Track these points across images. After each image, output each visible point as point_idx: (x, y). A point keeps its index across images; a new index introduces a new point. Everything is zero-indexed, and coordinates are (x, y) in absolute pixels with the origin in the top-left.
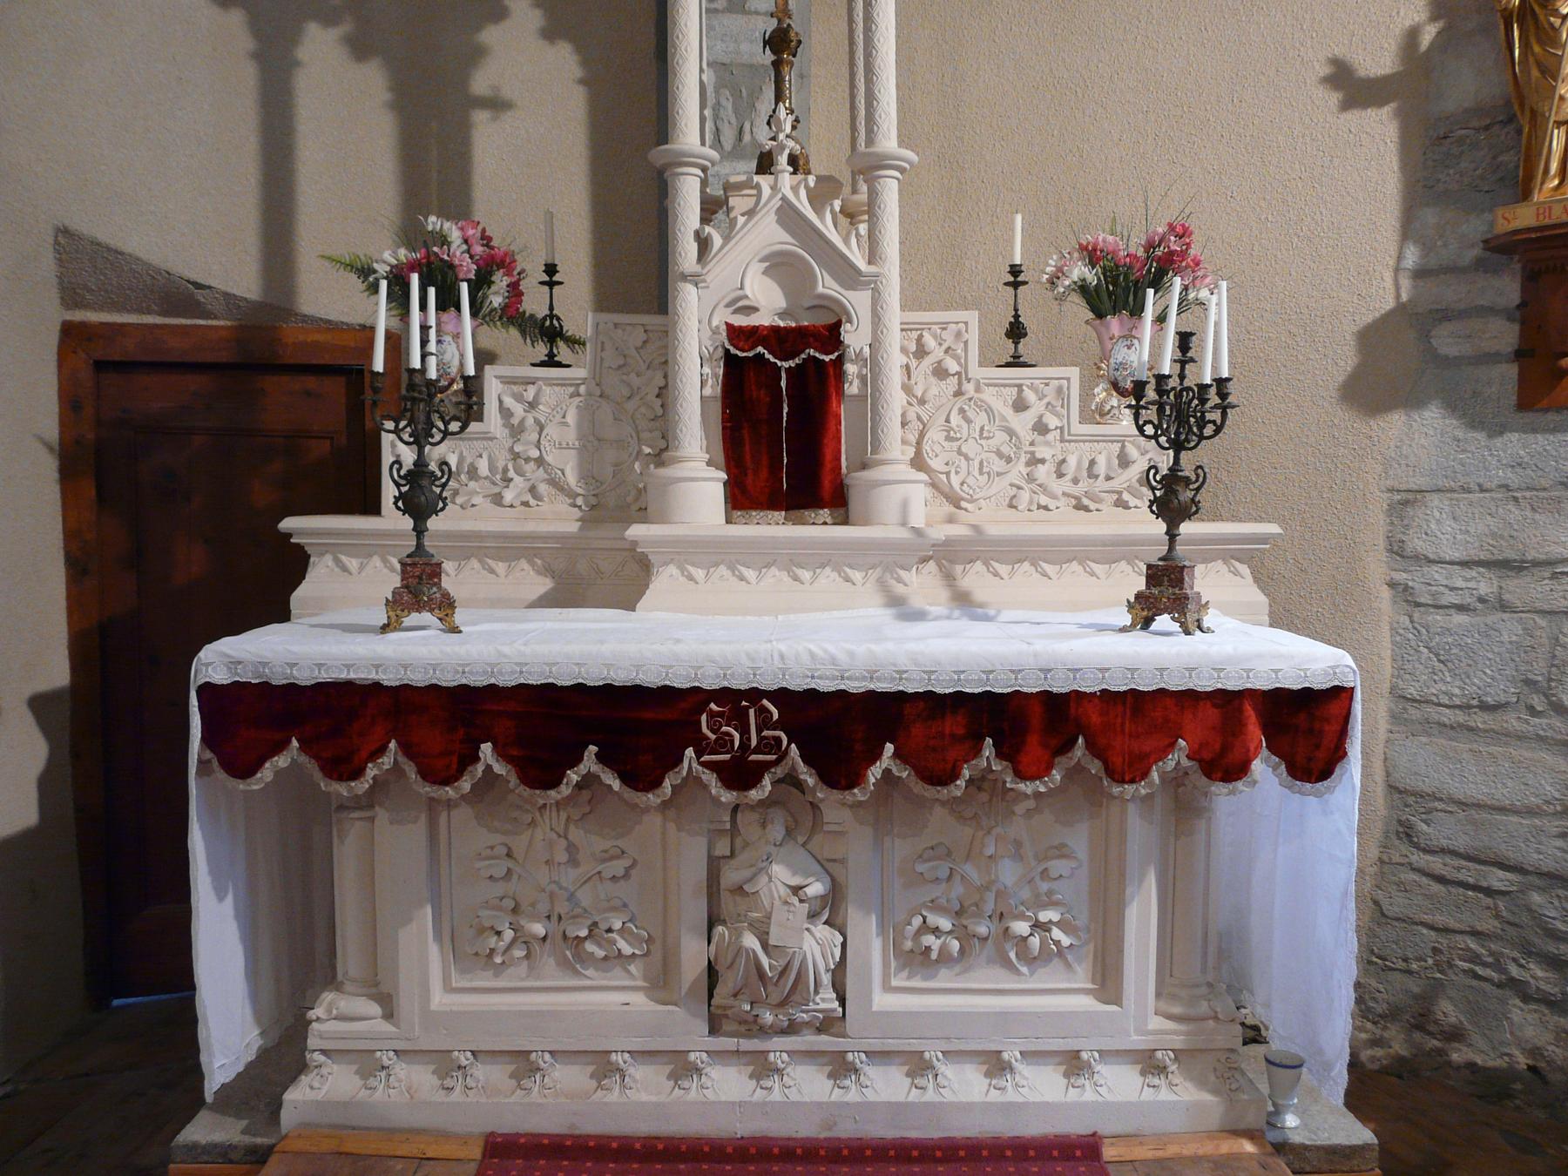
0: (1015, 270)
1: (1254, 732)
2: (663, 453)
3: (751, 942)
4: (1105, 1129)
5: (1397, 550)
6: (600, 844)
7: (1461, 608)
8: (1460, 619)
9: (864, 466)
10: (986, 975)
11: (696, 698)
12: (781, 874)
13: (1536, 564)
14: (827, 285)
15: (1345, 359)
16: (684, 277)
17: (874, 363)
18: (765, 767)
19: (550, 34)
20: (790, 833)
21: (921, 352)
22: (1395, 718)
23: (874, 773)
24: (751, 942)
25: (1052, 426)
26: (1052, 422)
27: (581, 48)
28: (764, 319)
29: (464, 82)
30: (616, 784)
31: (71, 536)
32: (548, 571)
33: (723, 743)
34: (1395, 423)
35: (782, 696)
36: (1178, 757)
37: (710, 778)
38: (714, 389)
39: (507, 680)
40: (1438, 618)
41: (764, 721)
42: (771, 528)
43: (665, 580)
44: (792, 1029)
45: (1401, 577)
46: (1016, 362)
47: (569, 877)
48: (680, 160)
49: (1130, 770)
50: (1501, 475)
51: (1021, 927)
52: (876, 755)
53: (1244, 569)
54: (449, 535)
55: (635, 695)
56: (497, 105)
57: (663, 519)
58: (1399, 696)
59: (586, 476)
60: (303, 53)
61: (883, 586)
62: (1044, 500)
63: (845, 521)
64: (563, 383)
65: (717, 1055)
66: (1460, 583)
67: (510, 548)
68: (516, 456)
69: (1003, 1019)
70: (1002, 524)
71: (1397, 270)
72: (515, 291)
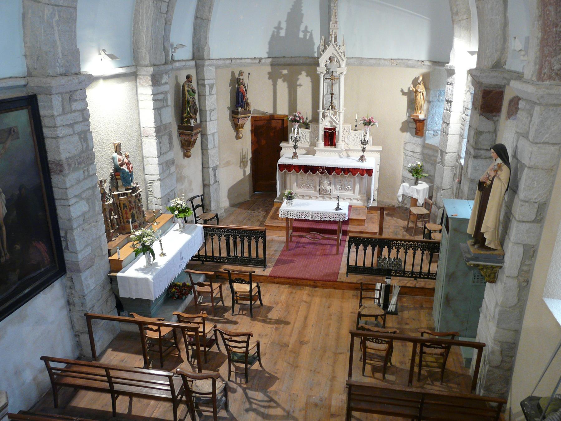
2: (318, 140)
3: (323, 187)
5: (404, 149)
8: (410, 157)
10: (343, 191)
11: (319, 167)
12: (326, 181)
14: (334, 124)
15: (401, 126)
19: (307, 76)
22: (403, 168)
24: (323, 187)
26: (358, 137)
27: (311, 77)
28: (328, 127)
29: (296, 83)
31: (252, 140)
32: (306, 150)
35: (325, 167)
38: (323, 134)
39: (303, 165)
40: (407, 157)
42: (329, 148)
43: (317, 153)
44: (326, 195)
46: (356, 130)
47: (308, 181)
49: (354, 174)
50: (414, 142)
51: (346, 187)
52: (333, 172)
55: (313, 166)
56: (300, 85)
57: (317, 147)
58: (404, 166)
59: (310, 141)
65: (320, 197)
67: (302, 148)
69: (344, 195)
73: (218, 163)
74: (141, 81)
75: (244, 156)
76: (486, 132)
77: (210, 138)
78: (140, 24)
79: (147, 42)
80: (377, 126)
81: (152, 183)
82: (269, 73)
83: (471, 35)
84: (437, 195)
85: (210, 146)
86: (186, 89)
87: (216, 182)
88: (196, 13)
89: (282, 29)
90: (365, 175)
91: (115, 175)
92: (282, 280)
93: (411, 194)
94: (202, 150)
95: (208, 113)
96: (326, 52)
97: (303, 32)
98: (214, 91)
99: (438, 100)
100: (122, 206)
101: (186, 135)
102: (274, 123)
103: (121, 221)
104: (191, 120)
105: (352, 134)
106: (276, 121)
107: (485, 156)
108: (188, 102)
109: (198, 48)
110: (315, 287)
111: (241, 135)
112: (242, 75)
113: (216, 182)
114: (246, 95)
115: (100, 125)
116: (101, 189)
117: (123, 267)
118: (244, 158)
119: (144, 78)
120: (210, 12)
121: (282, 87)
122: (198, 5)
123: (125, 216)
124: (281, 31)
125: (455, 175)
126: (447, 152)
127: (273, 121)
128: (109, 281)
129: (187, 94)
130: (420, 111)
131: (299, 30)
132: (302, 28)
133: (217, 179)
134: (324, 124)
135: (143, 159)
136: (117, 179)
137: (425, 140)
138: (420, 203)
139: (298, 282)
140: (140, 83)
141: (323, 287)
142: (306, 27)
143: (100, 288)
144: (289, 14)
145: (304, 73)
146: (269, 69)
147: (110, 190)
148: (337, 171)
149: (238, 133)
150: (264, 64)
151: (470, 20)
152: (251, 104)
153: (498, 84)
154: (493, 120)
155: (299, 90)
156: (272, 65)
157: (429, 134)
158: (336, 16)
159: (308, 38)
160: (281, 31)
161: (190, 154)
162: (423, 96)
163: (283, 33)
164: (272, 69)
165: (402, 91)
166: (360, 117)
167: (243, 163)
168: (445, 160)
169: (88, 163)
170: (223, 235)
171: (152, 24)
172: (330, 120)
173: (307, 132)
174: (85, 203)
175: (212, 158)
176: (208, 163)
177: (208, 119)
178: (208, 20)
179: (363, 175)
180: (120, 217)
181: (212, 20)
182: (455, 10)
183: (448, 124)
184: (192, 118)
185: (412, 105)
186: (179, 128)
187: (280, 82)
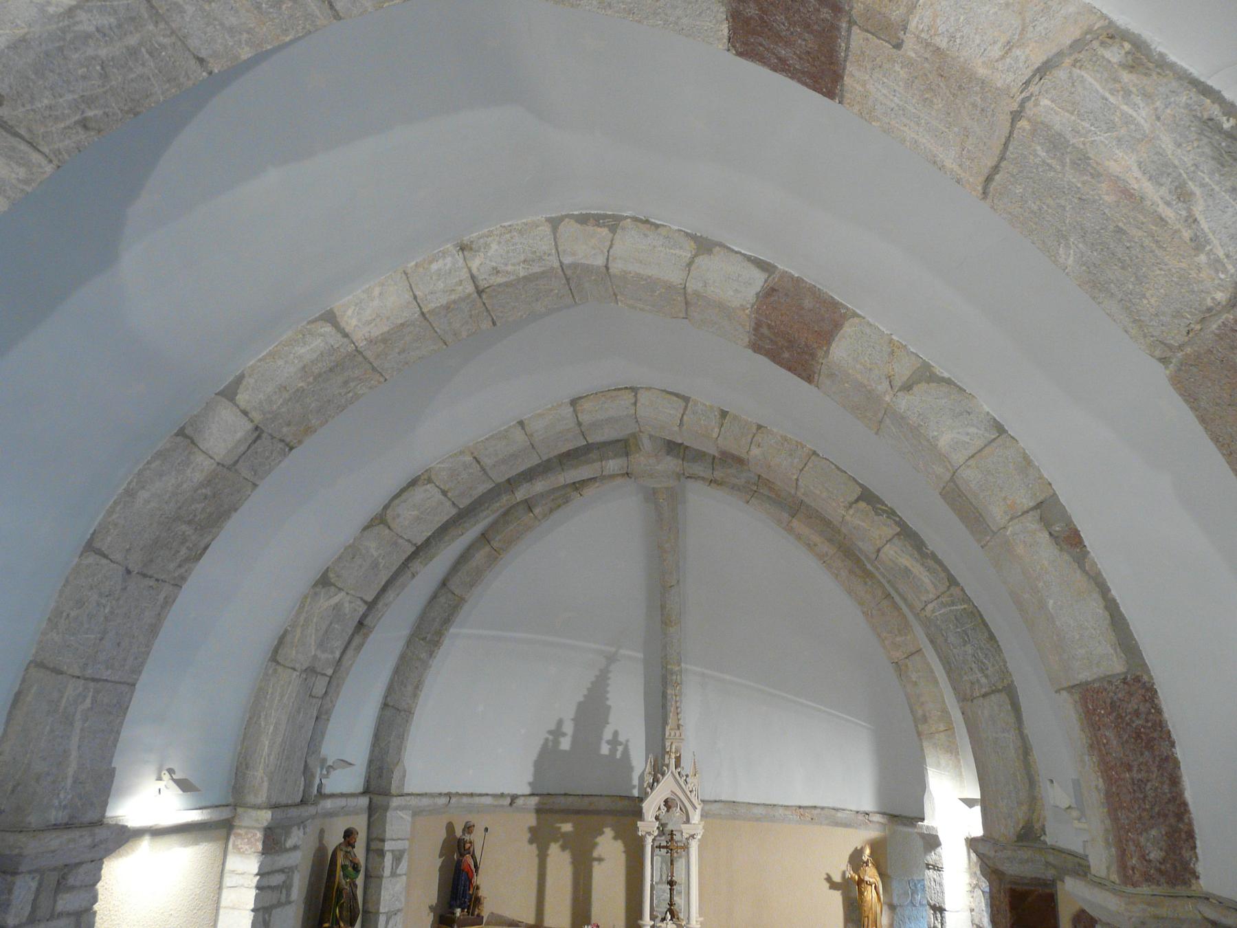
19: (615, 838)
25: (1136, 707)
29: (591, 853)
56: (600, 860)
60: (549, 852)
74: (239, 842)
79: (269, 755)
82: (531, 830)
88: (386, 697)
89: (564, 735)
96: (659, 788)
97: (608, 742)
98: (403, 867)
108: (340, 891)
109: (381, 768)
112: (470, 833)
114: (474, 880)
120: (415, 696)
121: (560, 863)
124: (562, 739)
129: (339, 873)
132: (607, 734)
142: (616, 734)
145: (609, 832)
146: (532, 820)
155: (598, 871)
159: (618, 755)
163: (565, 744)
165: (829, 879)
182: (920, 713)
187: (554, 849)
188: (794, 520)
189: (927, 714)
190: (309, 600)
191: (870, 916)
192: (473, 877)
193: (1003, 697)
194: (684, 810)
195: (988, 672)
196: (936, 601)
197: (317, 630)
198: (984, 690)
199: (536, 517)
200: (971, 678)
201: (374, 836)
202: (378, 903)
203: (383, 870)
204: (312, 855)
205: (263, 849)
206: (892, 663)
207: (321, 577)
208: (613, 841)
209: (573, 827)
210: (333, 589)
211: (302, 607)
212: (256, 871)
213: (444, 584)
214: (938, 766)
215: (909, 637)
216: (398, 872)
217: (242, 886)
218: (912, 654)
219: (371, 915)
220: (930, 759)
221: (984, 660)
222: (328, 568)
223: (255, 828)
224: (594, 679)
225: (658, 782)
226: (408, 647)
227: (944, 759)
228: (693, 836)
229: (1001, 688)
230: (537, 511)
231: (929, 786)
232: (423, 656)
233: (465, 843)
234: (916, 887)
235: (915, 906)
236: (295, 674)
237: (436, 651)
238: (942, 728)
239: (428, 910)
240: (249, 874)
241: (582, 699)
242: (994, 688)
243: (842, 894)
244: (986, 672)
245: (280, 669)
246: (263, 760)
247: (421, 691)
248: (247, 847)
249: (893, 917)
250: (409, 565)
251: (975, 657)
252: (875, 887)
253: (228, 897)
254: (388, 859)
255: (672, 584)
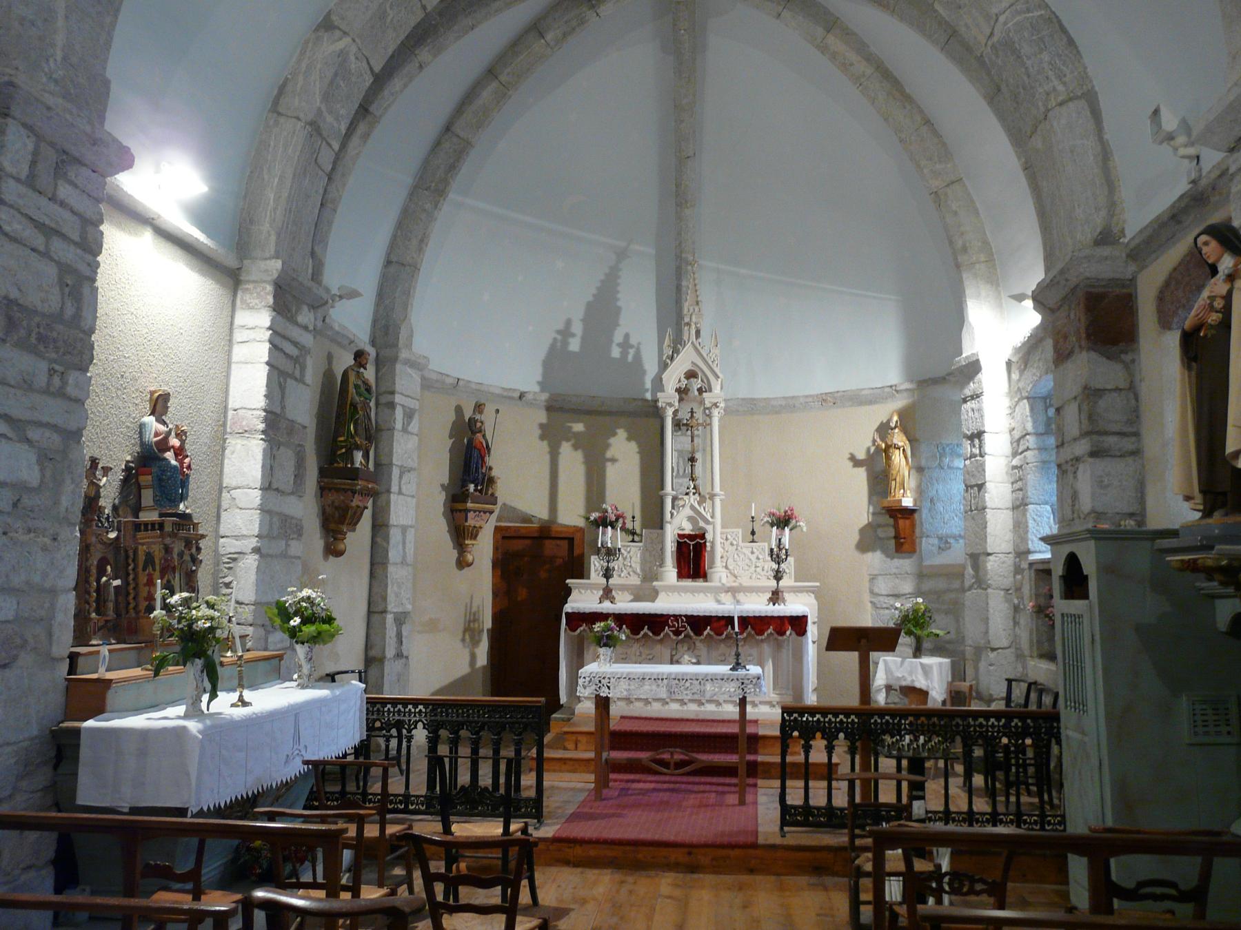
0: (753, 518)
1: (786, 622)
2: (662, 564)
4: (760, 718)
5: (872, 592)
6: (647, 652)
7: (887, 608)
8: (887, 611)
9: (711, 568)
11: (668, 616)
13: (903, 595)
14: (702, 524)
15: (856, 537)
16: (667, 522)
17: (713, 543)
18: (682, 631)
19: (629, 439)
20: (689, 649)
21: (727, 539)
23: (705, 633)
26: (761, 557)
27: (636, 441)
28: (687, 532)
30: (651, 634)
31: (493, 585)
32: (631, 594)
33: (674, 626)
34: (870, 555)
35: (686, 616)
36: (770, 630)
37: (671, 634)
38: (674, 549)
40: (882, 612)
41: (682, 621)
42: (688, 583)
43: (662, 596)
45: (873, 600)
46: (753, 541)
48: (666, 495)
50: (894, 570)
52: (706, 629)
53: (813, 595)
54: (614, 585)
56: (613, 460)
57: (662, 580)
59: (642, 570)
61: (715, 596)
62: (759, 577)
63: (707, 581)
64: (637, 547)
66: (886, 601)
68: (625, 565)
70: (745, 582)
71: (868, 512)
72: (624, 523)
73: (409, 607)
74: (247, 297)
75: (474, 614)
76: (1110, 390)
77: (395, 535)
78: (265, 171)
79: (275, 209)
80: (805, 529)
81: (234, 560)
82: (542, 426)
83: (1001, 299)
84: (977, 669)
85: (393, 555)
86: (352, 378)
87: (399, 655)
88: (388, 254)
89: (573, 335)
90: (788, 633)
91: (137, 474)
92: (593, 852)
93: (909, 679)
94: (372, 564)
95: (395, 472)
96: (679, 359)
97: (619, 345)
98: (414, 426)
99: (939, 464)
100: (142, 557)
101: (338, 490)
102: (549, 547)
103: (129, 603)
104: (355, 452)
105: (744, 550)
106: (554, 542)
107: (1120, 450)
108: (354, 406)
109: (387, 327)
110: (693, 868)
111: (470, 558)
112: (481, 412)
113: (399, 655)
114: (487, 458)
115: (122, 326)
116: (92, 483)
117: (108, 708)
118: (474, 621)
119: (255, 288)
120: (420, 250)
121: (572, 462)
122: (394, 237)
123: (144, 592)
124: (571, 340)
125: (1016, 609)
126: (989, 551)
127: (547, 542)
128: (53, 753)
129: (352, 390)
130: (902, 491)
131: (610, 341)
132: (618, 337)
133: (404, 647)
134: (678, 524)
135: (220, 492)
136: (139, 488)
137: (921, 559)
138: (935, 700)
139: (640, 856)
140: (243, 301)
141: (717, 868)
142: (627, 336)
143: (13, 761)
144: (589, 305)
145: (622, 434)
146: (542, 417)
147: (115, 508)
148: (715, 625)
149: (461, 547)
150: (531, 404)
151: (995, 265)
152: (498, 481)
153: (1118, 276)
154: (1123, 362)
155: (611, 472)
156: (550, 408)
157: (927, 545)
158: (696, 291)
159: (630, 358)
160: (571, 340)
161: (341, 547)
162: (906, 457)
163: (574, 345)
164: (548, 418)
165: (852, 458)
166: (760, 509)
167: (470, 631)
168: (986, 572)
169: (67, 357)
170: (420, 725)
171: (294, 175)
172: (691, 513)
173: (633, 550)
174: (33, 458)
175: (395, 588)
176: (385, 599)
177: (394, 488)
178: (416, 268)
179: (782, 633)
180: (128, 584)
181: (424, 268)
182: (959, 244)
183: (981, 487)
184: (358, 448)
185: (880, 480)
186: (323, 473)
187: (566, 448)
188: (830, 35)
189: (968, 245)
190: (310, 45)
191: (898, 480)
192: (485, 456)
193: (1082, 103)
194: (705, 381)
195: (1067, 79)
196: (1009, 10)
197: (321, 78)
198: (1060, 99)
199: (548, 44)
200: (1046, 88)
201: (383, 389)
202: (391, 454)
203: (395, 423)
204: (322, 375)
205: (274, 303)
206: (931, 194)
207: (324, 19)
208: (627, 442)
209: (585, 427)
210: (337, 33)
211: (303, 53)
212: (268, 324)
213: (448, 128)
214: (978, 296)
215: (949, 166)
216: (410, 429)
217: (254, 340)
218: (953, 183)
219: (384, 467)
220: (969, 291)
221: (1062, 67)
222: (330, 11)
223: (265, 282)
224: (602, 277)
225: (678, 353)
226: (411, 200)
227: (985, 289)
228: (716, 405)
229: (1079, 94)
230: (550, 36)
231: (968, 318)
232: (428, 206)
233: (476, 421)
234: (944, 451)
235: (942, 468)
236: (300, 125)
237: (442, 202)
238: (983, 259)
239: (440, 489)
240: (261, 328)
241: (591, 299)
242: (1072, 95)
243: (868, 470)
244: (1064, 79)
245: (282, 120)
246: (268, 214)
247: (427, 245)
248: (257, 301)
249: (921, 479)
250: (416, 52)
251: (1052, 65)
252: (904, 450)
253: (238, 352)
254: (399, 413)
255: (689, 155)
